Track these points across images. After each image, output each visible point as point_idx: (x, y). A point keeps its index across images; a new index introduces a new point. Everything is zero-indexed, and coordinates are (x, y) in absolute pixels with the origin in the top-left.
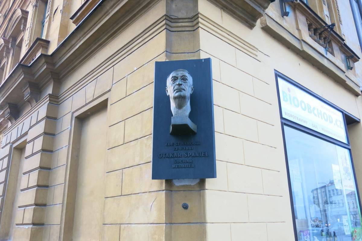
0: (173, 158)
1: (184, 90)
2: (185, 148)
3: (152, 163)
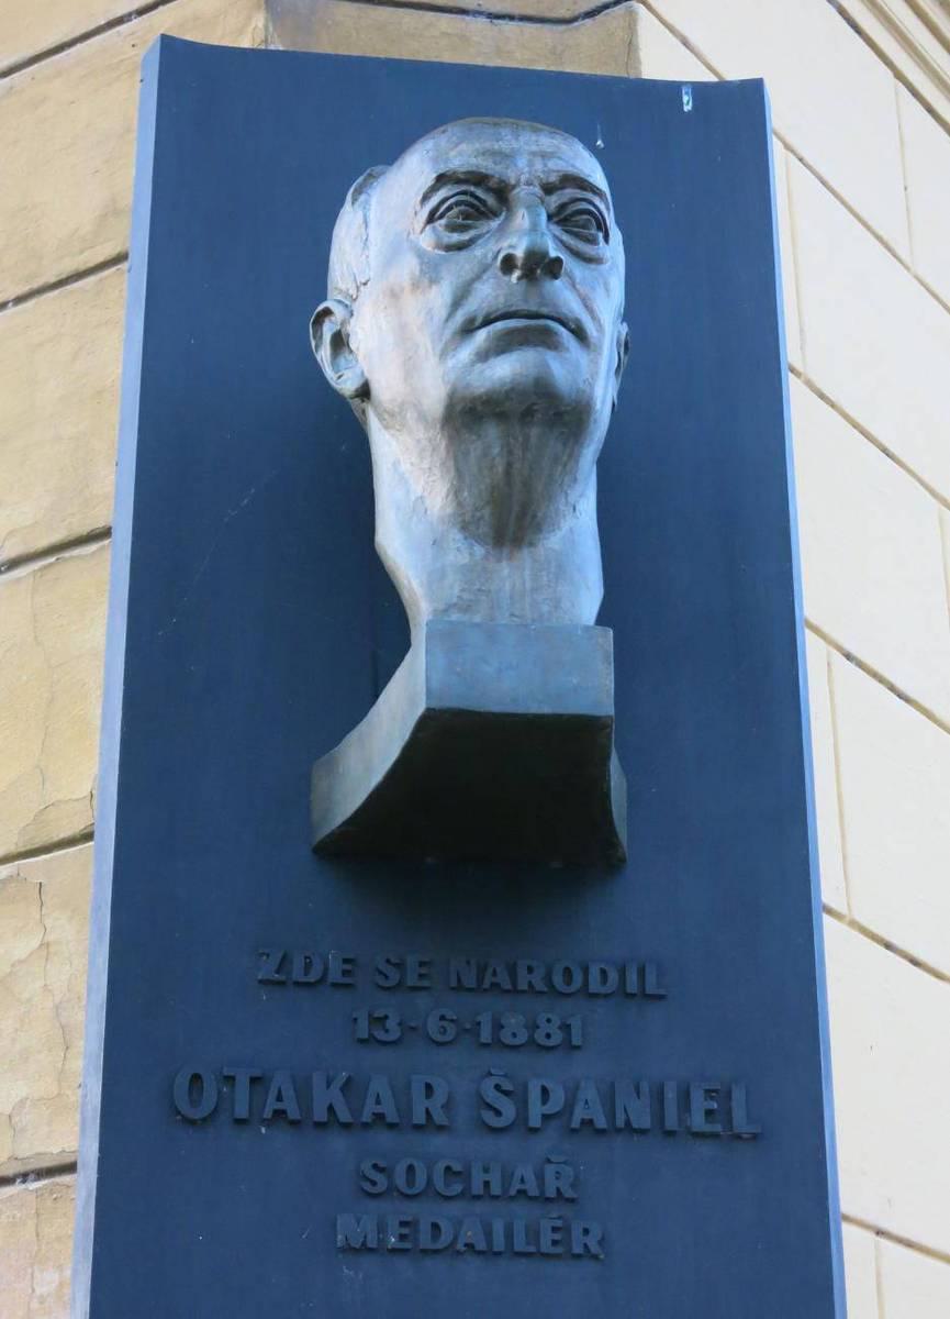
0: (346, 1126)
1: (579, 333)
2: (498, 1026)
3: (84, 1185)
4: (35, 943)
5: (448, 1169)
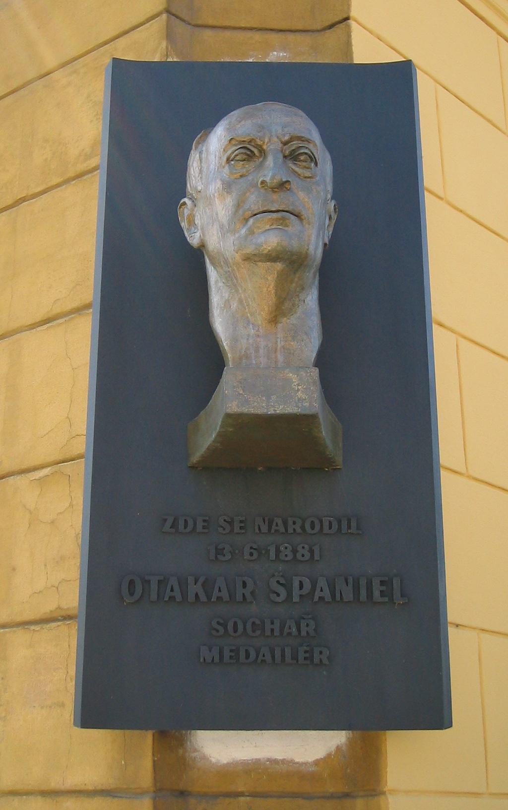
4: (67, 504)
5: (254, 623)
